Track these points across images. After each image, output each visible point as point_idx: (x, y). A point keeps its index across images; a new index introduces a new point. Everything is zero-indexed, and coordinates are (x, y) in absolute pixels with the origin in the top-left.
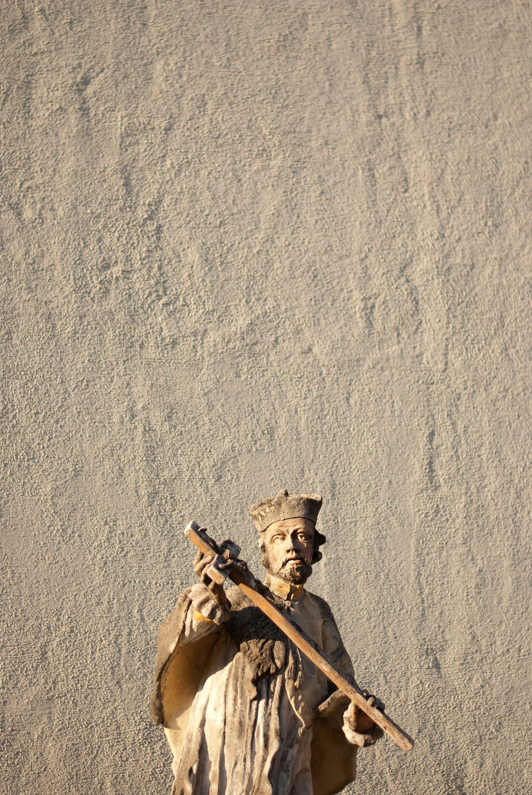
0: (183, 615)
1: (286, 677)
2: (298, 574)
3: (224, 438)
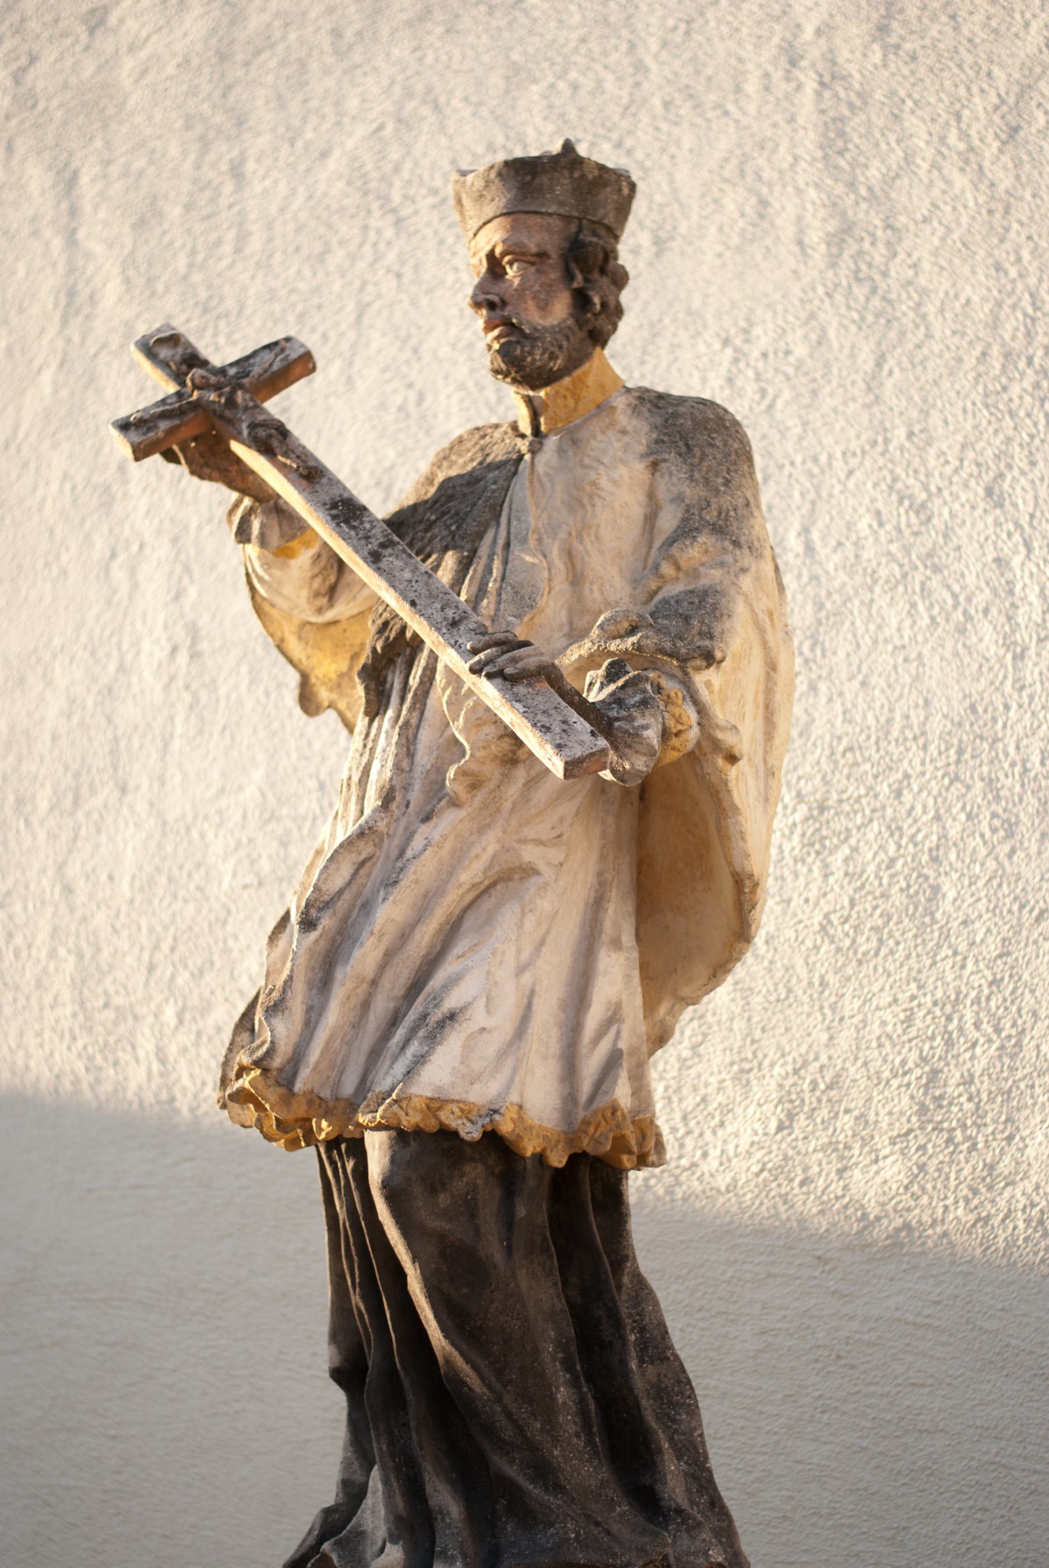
3: (1027, 25)
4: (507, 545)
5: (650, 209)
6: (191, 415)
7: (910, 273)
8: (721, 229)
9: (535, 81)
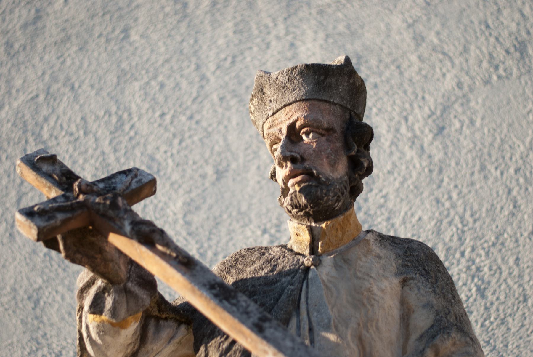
3: (444, 75)
4: (311, 330)
5: (212, 153)
6: (79, 212)
7: (382, 201)
8: (258, 168)
9: (136, 79)
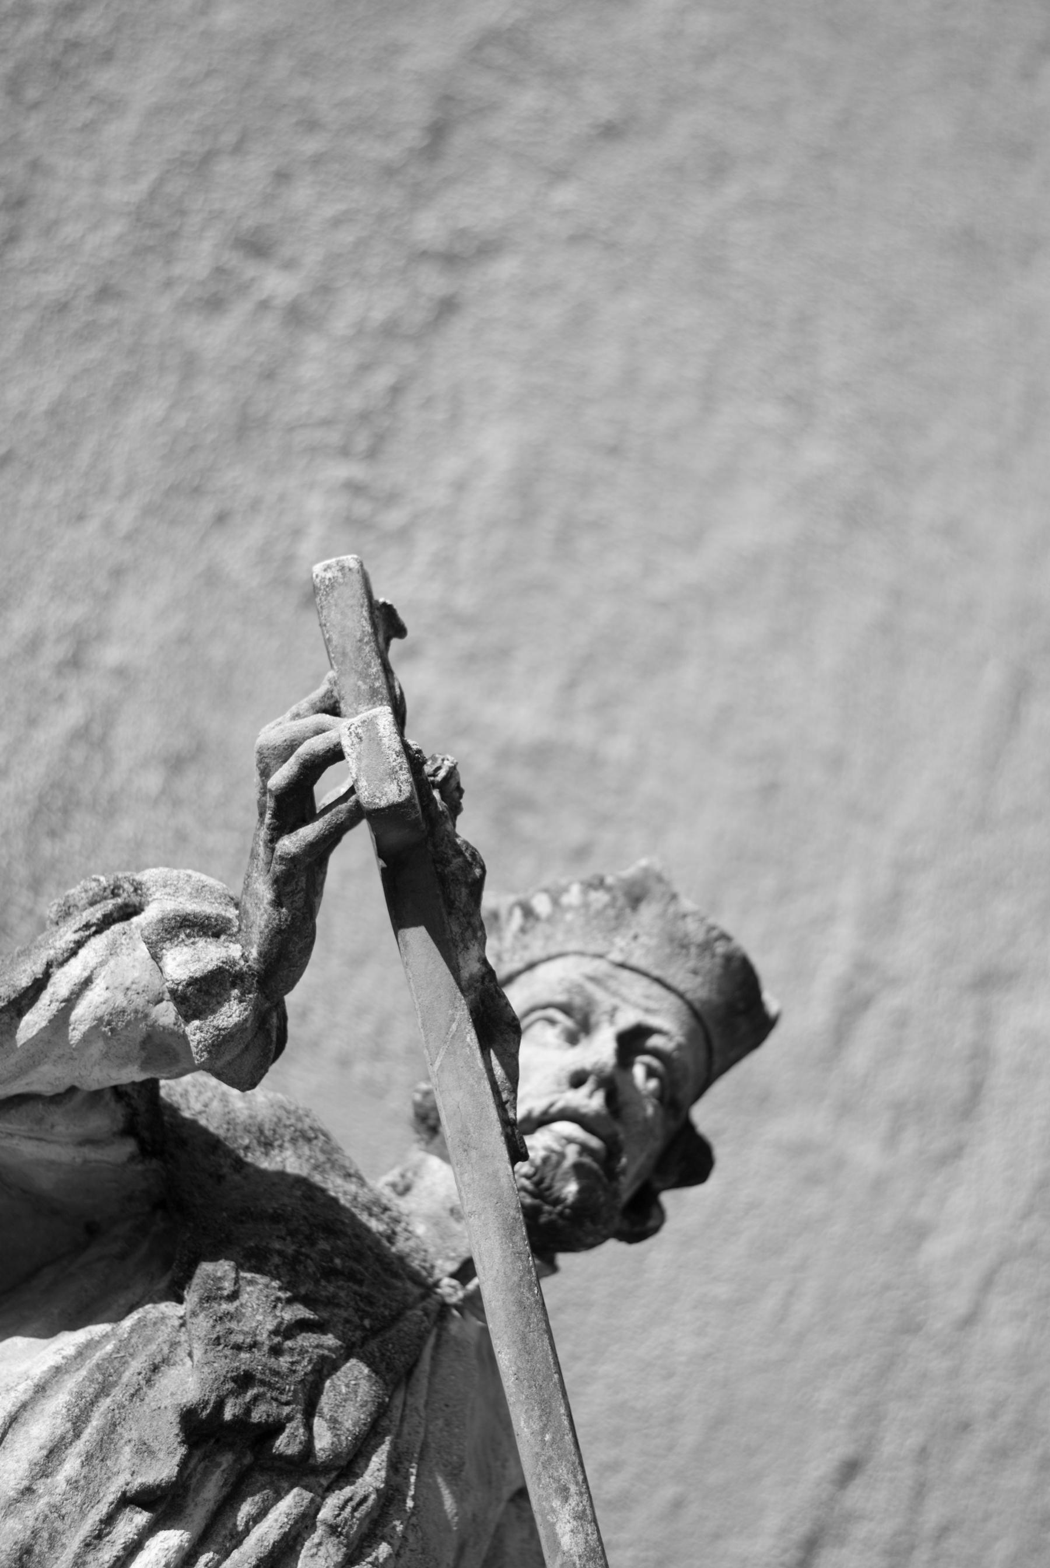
0: (67, 935)
1: (325, 1513)
2: (571, 1189)
